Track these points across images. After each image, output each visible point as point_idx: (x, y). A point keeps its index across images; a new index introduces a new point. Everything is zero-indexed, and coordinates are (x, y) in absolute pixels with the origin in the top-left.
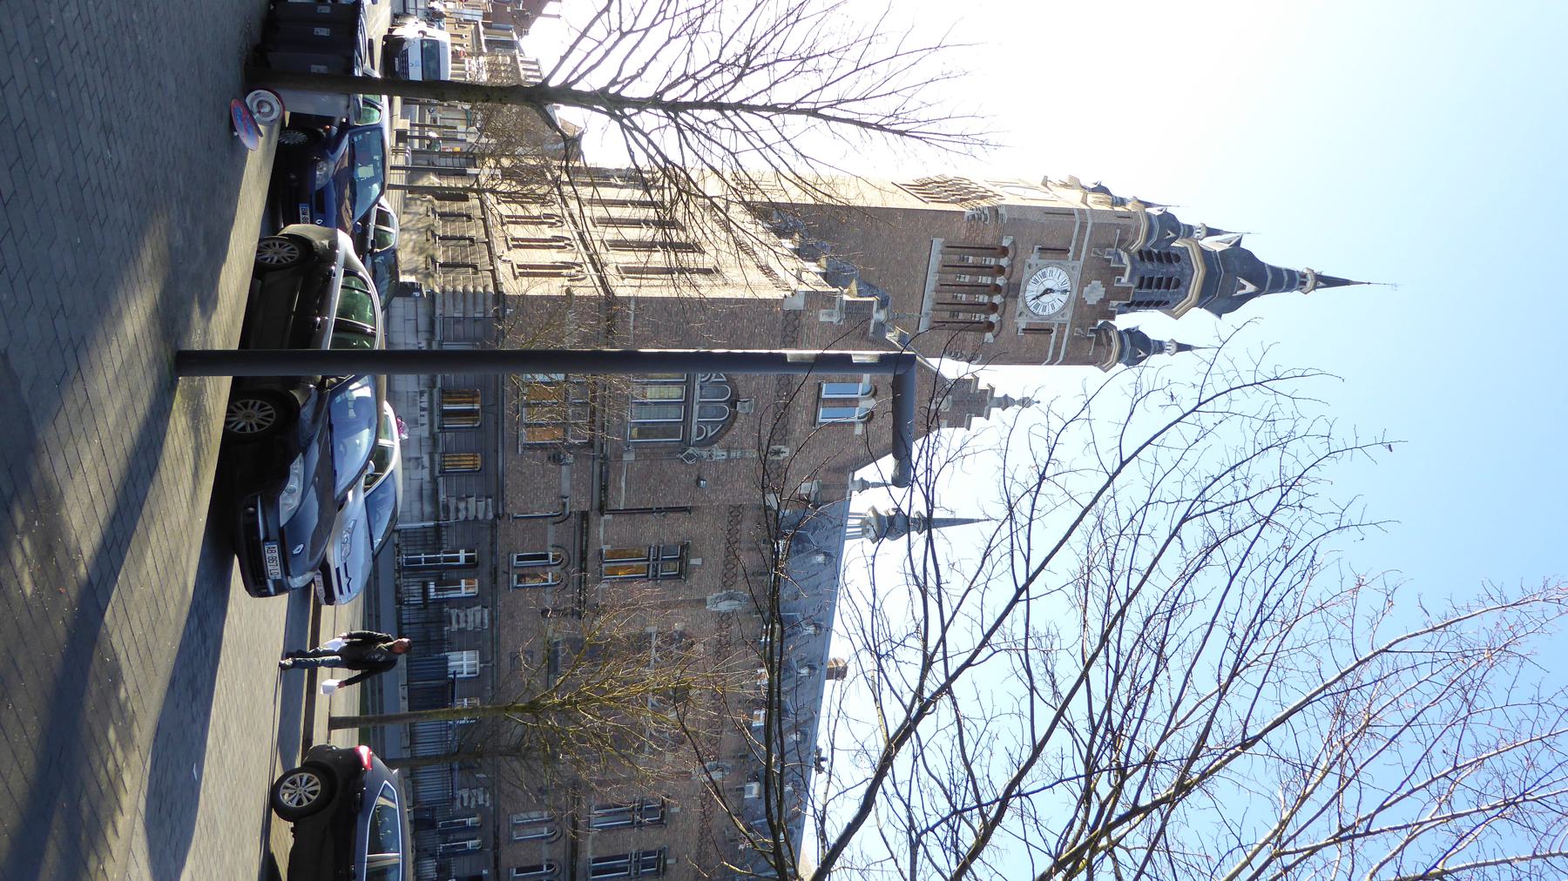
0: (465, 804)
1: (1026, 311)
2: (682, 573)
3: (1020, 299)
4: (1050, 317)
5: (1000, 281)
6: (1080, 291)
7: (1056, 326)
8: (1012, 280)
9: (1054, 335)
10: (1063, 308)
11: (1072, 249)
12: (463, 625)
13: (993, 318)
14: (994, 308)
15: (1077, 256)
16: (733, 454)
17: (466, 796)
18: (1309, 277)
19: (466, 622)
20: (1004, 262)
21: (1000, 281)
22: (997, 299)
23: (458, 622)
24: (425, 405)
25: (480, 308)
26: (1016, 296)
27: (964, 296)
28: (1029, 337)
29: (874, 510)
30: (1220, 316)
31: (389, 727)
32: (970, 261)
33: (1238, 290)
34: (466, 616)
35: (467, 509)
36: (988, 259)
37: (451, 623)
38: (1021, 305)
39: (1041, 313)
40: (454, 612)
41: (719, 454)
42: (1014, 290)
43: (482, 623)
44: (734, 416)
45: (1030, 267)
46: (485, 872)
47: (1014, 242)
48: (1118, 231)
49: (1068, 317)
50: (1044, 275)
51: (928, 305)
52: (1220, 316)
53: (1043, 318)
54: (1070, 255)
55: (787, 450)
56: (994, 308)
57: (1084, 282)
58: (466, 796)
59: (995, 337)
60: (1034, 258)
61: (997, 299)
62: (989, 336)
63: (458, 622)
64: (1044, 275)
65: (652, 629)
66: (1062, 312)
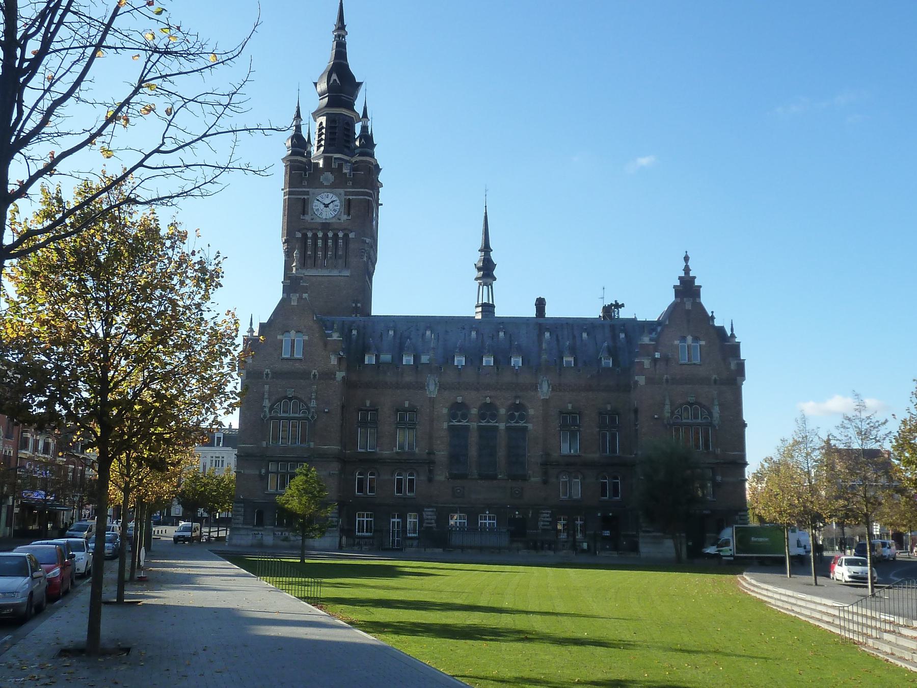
0: (548, 523)
1: (337, 216)
2: (413, 410)
3: (331, 221)
4: (341, 202)
5: (320, 235)
6: (326, 187)
7: (345, 197)
8: (320, 228)
9: (351, 197)
10: (336, 195)
11: (302, 197)
12: (433, 521)
13: (341, 235)
14: (336, 236)
15: (307, 193)
16: (313, 397)
17: (542, 523)
18: (340, 33)
19: (431, 519)
20: (310, 234)
21: (320, 235)
22: (330, 234)
23: (431, 523)
24: (280, 533)
25: (240, 509)
26: (329, 224)
27: (329, 253)
28: (352, 212)
29: (477, 279)
30: (360, 84)
31: (190, 533)
32: (310, 253)
33: (337, 82)
34: (427, 519)
35: (332, 517)
36: (308, 243)
37: (431, 527)
38: (334, 220)
39: (339, 208)
40: (425, 525)
41: (313, 404)
42: (326, 226)
43: (432, 511)
44: (296, 398)
45: (312, 219)
46: (599, 515)
47: (299, 231)
48: (293, 172)
49: (342, 191)
50: (317, 210)
51: (335, 273)
52: (360, 84)
53: (341, 206)
54: (306, 197)
55: (314, 371)
56: (336, 236)
57: (322, 186)
58: (542, 523)
59: (352, 232)
60: (307, 218)
61: (330, 234)
62: (352, 235)
63: (431, 523)
64: (317, 210)
65: (445, 425)
66: (339, 195)
